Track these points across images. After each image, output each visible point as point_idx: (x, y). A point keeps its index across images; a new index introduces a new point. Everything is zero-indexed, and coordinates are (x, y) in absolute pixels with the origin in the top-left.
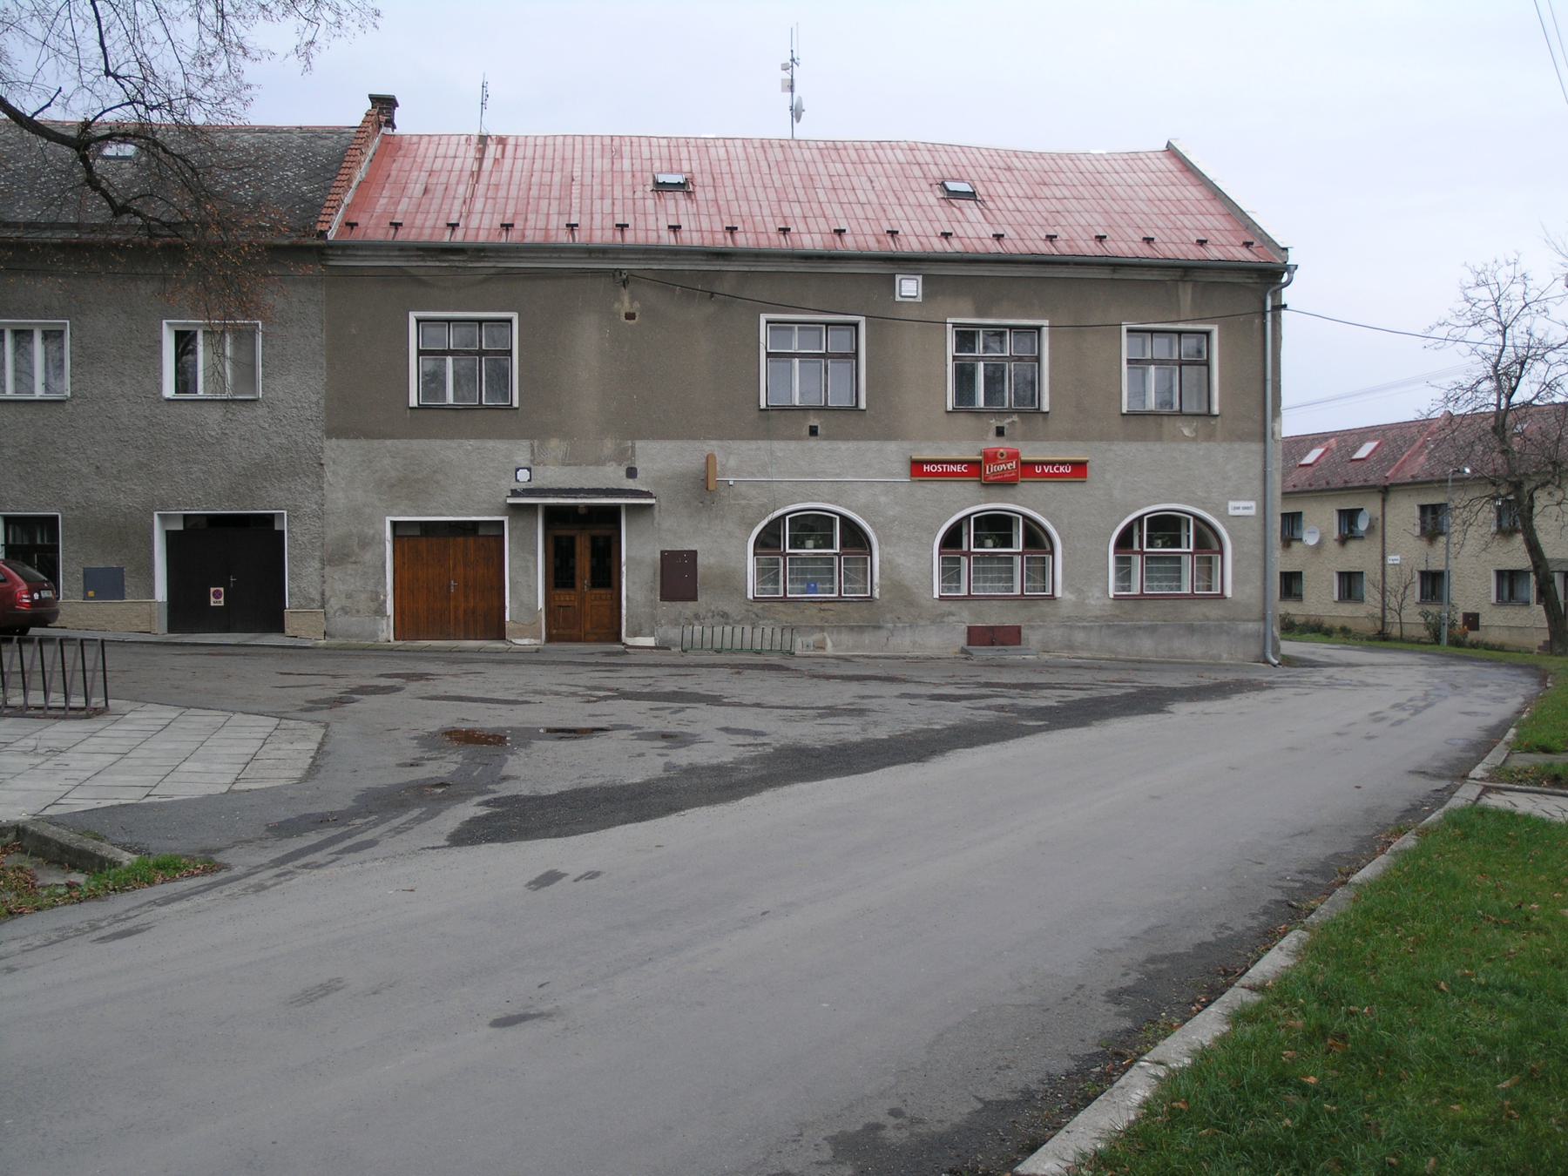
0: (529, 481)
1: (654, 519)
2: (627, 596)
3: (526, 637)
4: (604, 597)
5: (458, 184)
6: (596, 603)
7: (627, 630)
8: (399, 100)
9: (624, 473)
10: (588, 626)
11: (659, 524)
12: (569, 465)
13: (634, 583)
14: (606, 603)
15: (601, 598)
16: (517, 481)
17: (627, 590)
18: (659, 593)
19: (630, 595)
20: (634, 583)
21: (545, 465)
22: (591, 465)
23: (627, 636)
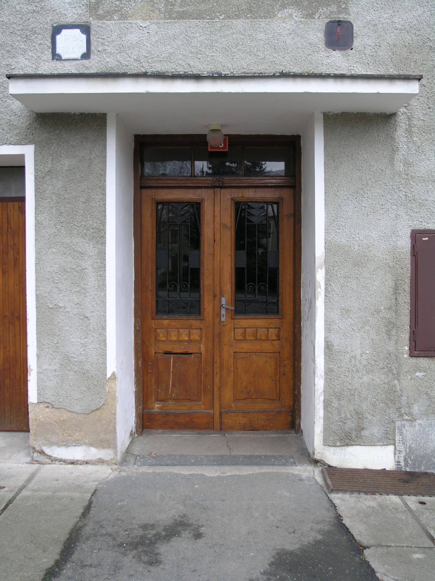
0: (86, 56)
1: (394, 150)
2: (328, 347)
3: (77, 443)
4: (262, 333)
5: (10, 368)
6: (245, 346)
7: (326, 429)
8: (301, 135)
9: (321, 36)
10: (228, 394)
11: (407, 164)
12: (182, 16)
13: (346, 311)
14: (267, 346)
15: (255, 335)
16: (56, 56)
17: (328, 329)
18: (405, 336)
19: (336, 340)
20: (346, 311)
21: (124, 17)
22: (238, 17)
23: (327, 443)
